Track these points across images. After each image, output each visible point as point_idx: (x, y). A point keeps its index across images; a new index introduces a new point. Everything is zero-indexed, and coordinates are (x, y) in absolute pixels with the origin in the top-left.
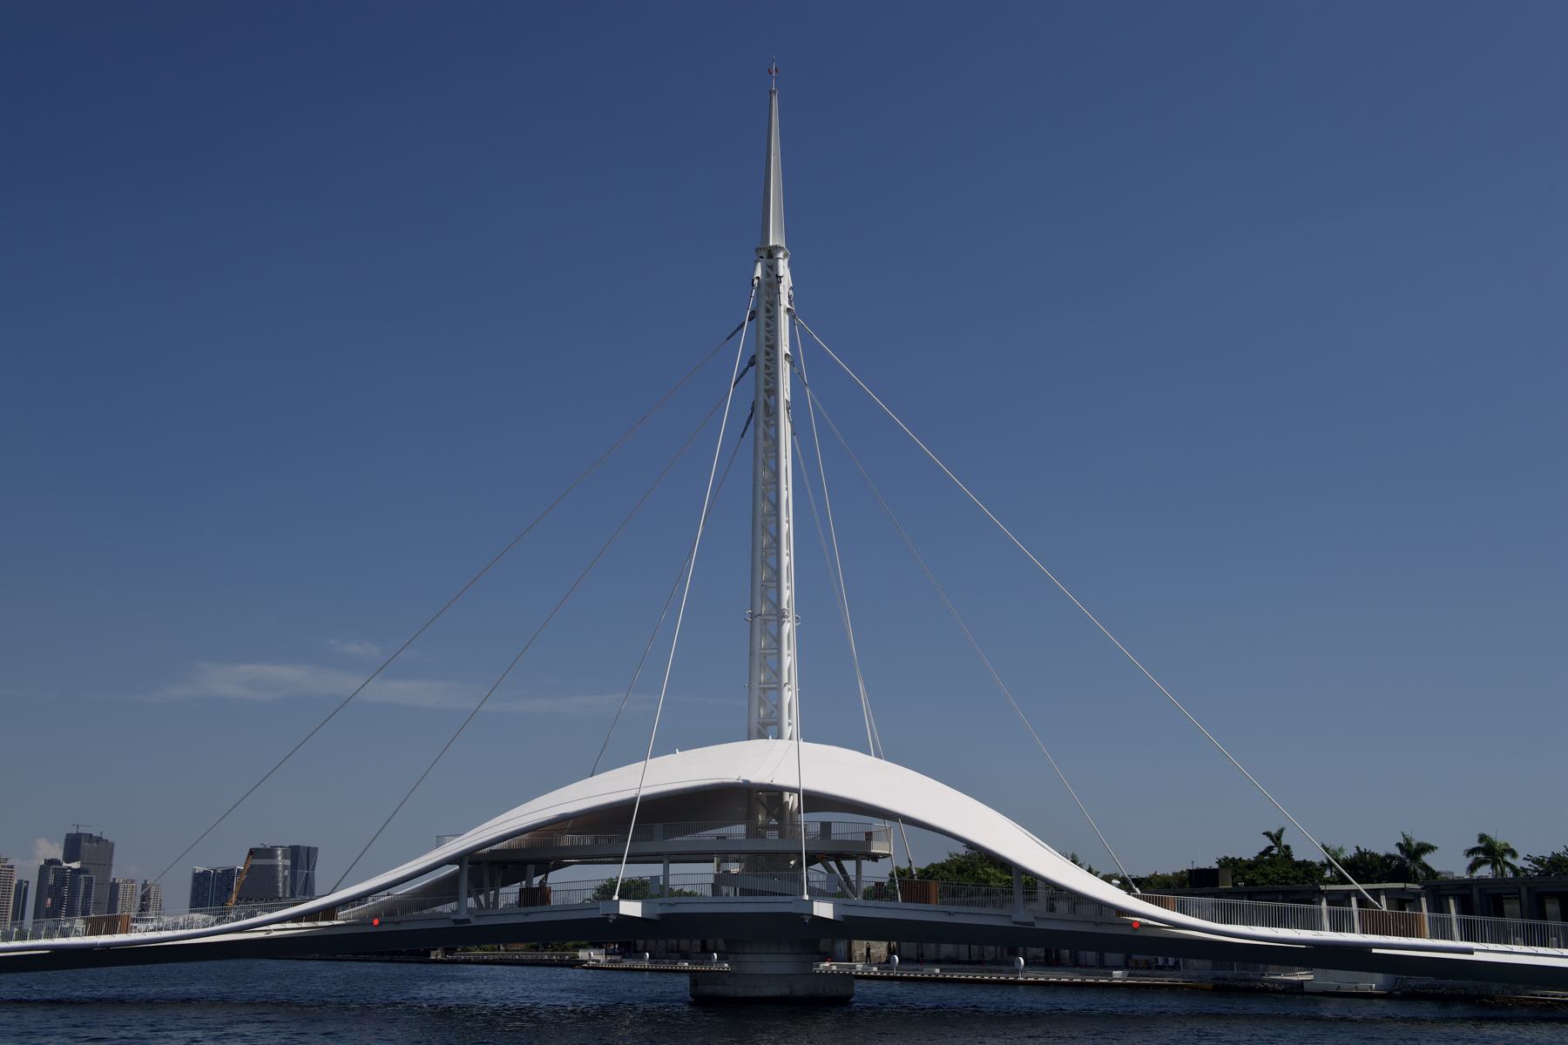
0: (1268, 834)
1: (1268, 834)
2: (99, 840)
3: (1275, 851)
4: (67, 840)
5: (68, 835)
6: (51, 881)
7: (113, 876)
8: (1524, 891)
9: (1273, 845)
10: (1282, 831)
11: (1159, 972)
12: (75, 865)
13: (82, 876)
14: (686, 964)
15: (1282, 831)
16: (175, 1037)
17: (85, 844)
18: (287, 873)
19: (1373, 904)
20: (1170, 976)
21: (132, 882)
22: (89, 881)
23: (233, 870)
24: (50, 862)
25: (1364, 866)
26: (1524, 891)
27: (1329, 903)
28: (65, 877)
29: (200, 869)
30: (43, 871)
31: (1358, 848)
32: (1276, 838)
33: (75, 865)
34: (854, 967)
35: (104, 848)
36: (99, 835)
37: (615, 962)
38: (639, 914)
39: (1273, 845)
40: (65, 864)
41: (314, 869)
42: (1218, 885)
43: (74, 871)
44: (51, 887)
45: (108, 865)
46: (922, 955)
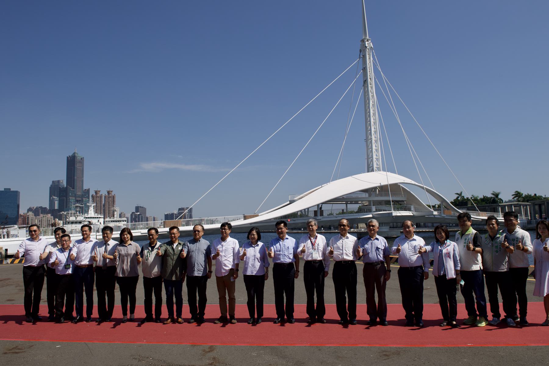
0: (457, 194)
1: (457, 194)
2: (143, 207)
3: (459, 199)
4: (136, 208)
5: (136, 207)
6: (134, 217)
7: (147, 215)
8: (546, 203)
9: (458, 196)
10: (461, 193)
11: (454, 227)
12: (138, 213)
13: (140, 216)
14: (337, 231)
15: (461, 193)
16: (56, 257)
17: (140, 209)
18: (187, 214)
19: (477, 210)
20: (456, 228)
21: (151, 217)
22: (142, 217)
23: (173, 213)
24: (133, 213)
25: (485, 200)
26: (546, 203)
27: (514, 207)
28: (136, 216)
29: (166, 214)
30: (131, 215)
31: (483, 196)
32: (460, 194)
33: (138, 213)
34: (361, 230)
35: (144, 209)
36: (380, 185)
37: (290, 231)
38: (372, 216)
39: (458, 196)
40: (136, 213)
41: (192, 213)
42: (467, 205)
43: (138, 214)
44: (134, 219)
45: (145, 213)
46: (397, 226)
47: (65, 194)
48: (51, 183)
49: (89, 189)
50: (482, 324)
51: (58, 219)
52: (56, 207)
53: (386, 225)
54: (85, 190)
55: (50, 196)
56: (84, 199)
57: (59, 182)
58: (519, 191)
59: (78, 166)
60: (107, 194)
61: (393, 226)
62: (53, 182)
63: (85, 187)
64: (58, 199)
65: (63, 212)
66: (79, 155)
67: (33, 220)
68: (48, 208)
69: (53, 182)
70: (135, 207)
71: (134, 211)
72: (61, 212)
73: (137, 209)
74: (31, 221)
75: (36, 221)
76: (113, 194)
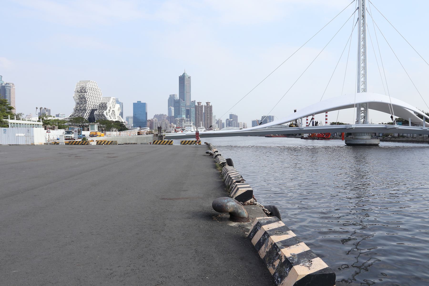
12: (232, 120)
21: (241, 123)
24: (227, 119)
33: (232, 120)
35: (236, 117)
47: (178, 105)
48: (169, 97)
49: (195, 101)
50: (233, 206)
51: (173, 124)
52: (173, 115)
53: (367, 135)
54: (192, 101)
55: (169, 106)
56: (191, 108)
57: (174, 96)
58: (233, 113)
59: (186, 83)
60: (206, 105)
61: (410, 136)
62: (170, 95)
63: (192, 100)
64: (174, 109)
65: (177, 118)
66: (188, 74)
67: (156, 124)
68: (167, 115)
69: (170, 95)
70: (237, 115)
71: (229, 118)
72: (176, 118)
73: (231, 116)
74: (155, 126)
75: (158, 124)
76: (201, 105)
